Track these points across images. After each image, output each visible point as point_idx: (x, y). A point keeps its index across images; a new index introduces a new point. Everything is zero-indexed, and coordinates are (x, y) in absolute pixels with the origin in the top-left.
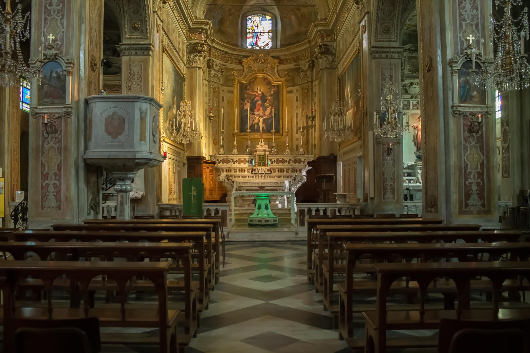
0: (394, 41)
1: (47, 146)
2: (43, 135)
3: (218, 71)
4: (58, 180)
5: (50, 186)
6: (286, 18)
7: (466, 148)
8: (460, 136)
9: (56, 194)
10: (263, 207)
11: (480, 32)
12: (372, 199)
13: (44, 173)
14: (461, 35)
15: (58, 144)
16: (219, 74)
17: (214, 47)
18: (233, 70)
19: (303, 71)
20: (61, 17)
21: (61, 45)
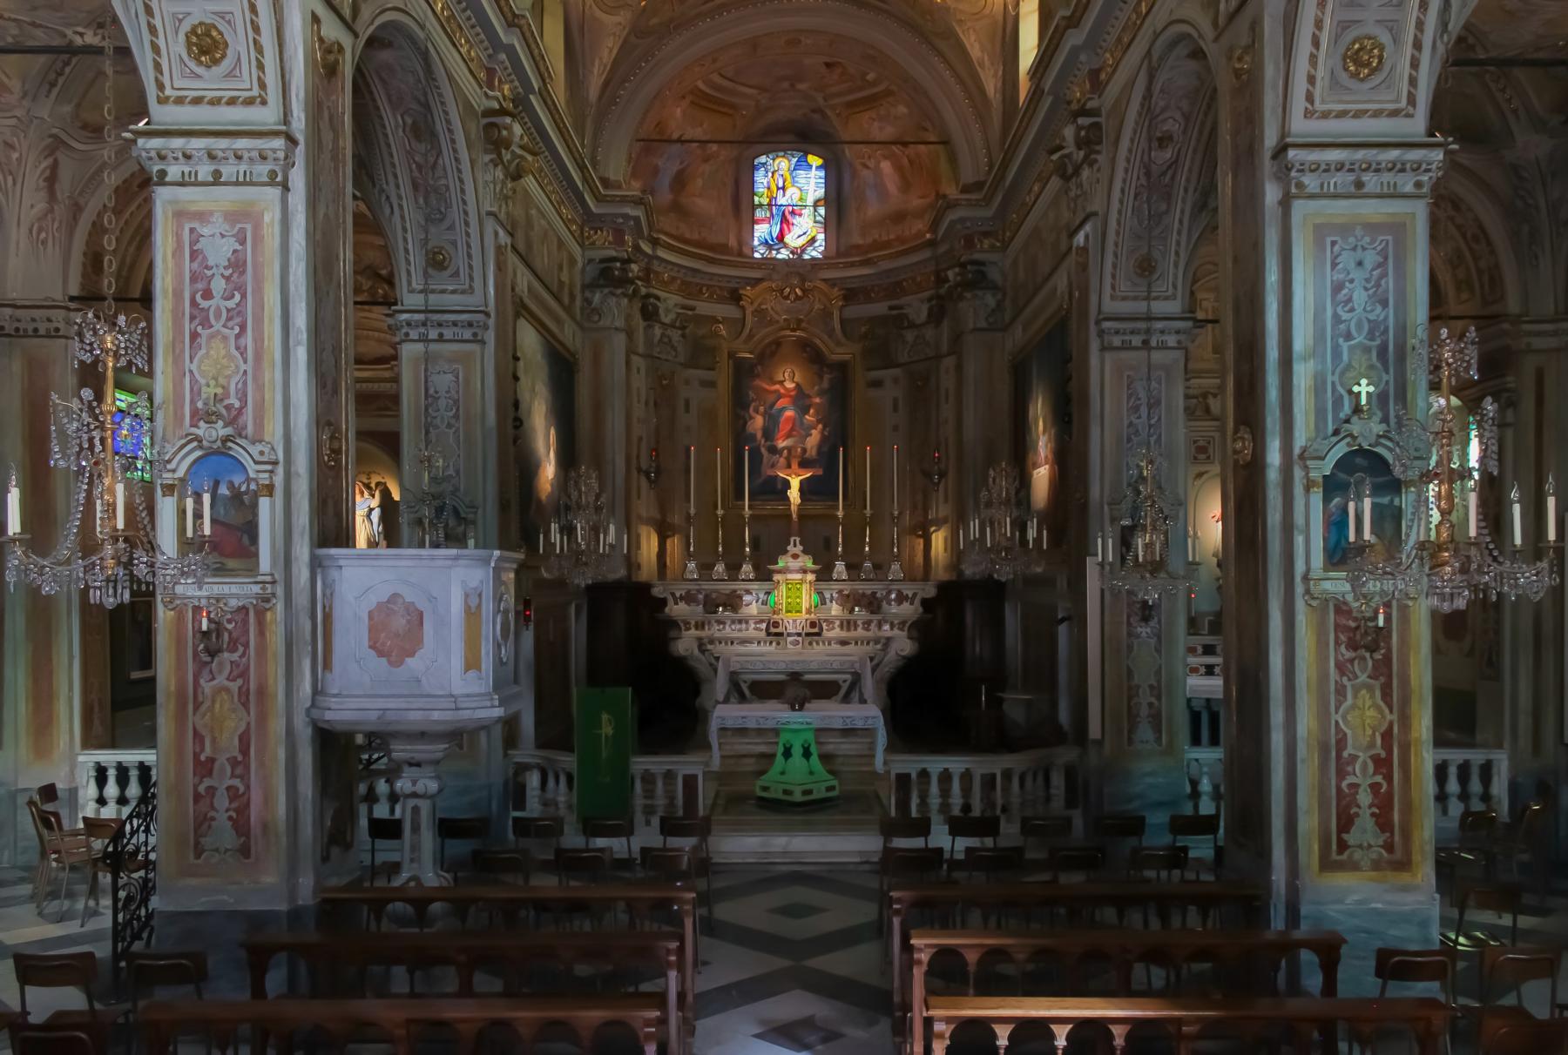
0: (1166, 298)
1: (207, 687)
2: (195, 654)
3: (672, 325)
4: (241, 777)
5: (218, 794)
6: (866, 167)
7: (1341, 691)
8: (1327, 658)
9: (234, 815)
10: (797, 751)
11: (1391, 371)
12: (1100, 743)
13: (203, 758)
14: (1336, 378)
15: (240, 682)
16: (675, 335)
17: (658, 258)
18: (714, 320)
19: (912, 326)
20: (237, 330)
21: (241, 409)
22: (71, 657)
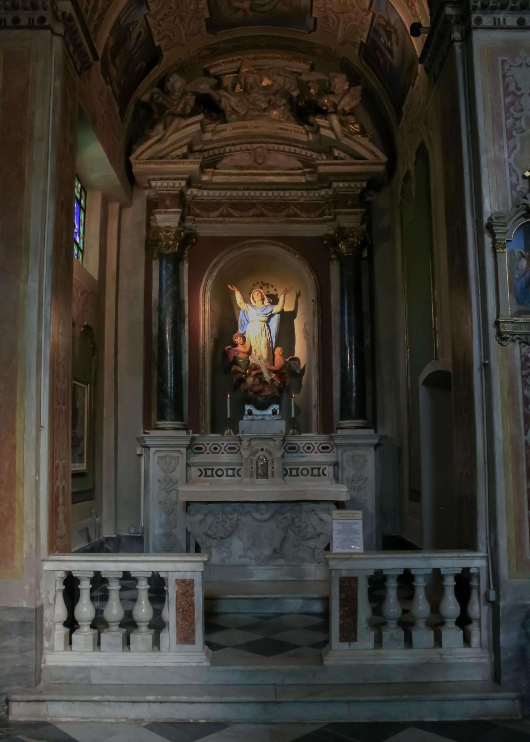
22: (39, 428)
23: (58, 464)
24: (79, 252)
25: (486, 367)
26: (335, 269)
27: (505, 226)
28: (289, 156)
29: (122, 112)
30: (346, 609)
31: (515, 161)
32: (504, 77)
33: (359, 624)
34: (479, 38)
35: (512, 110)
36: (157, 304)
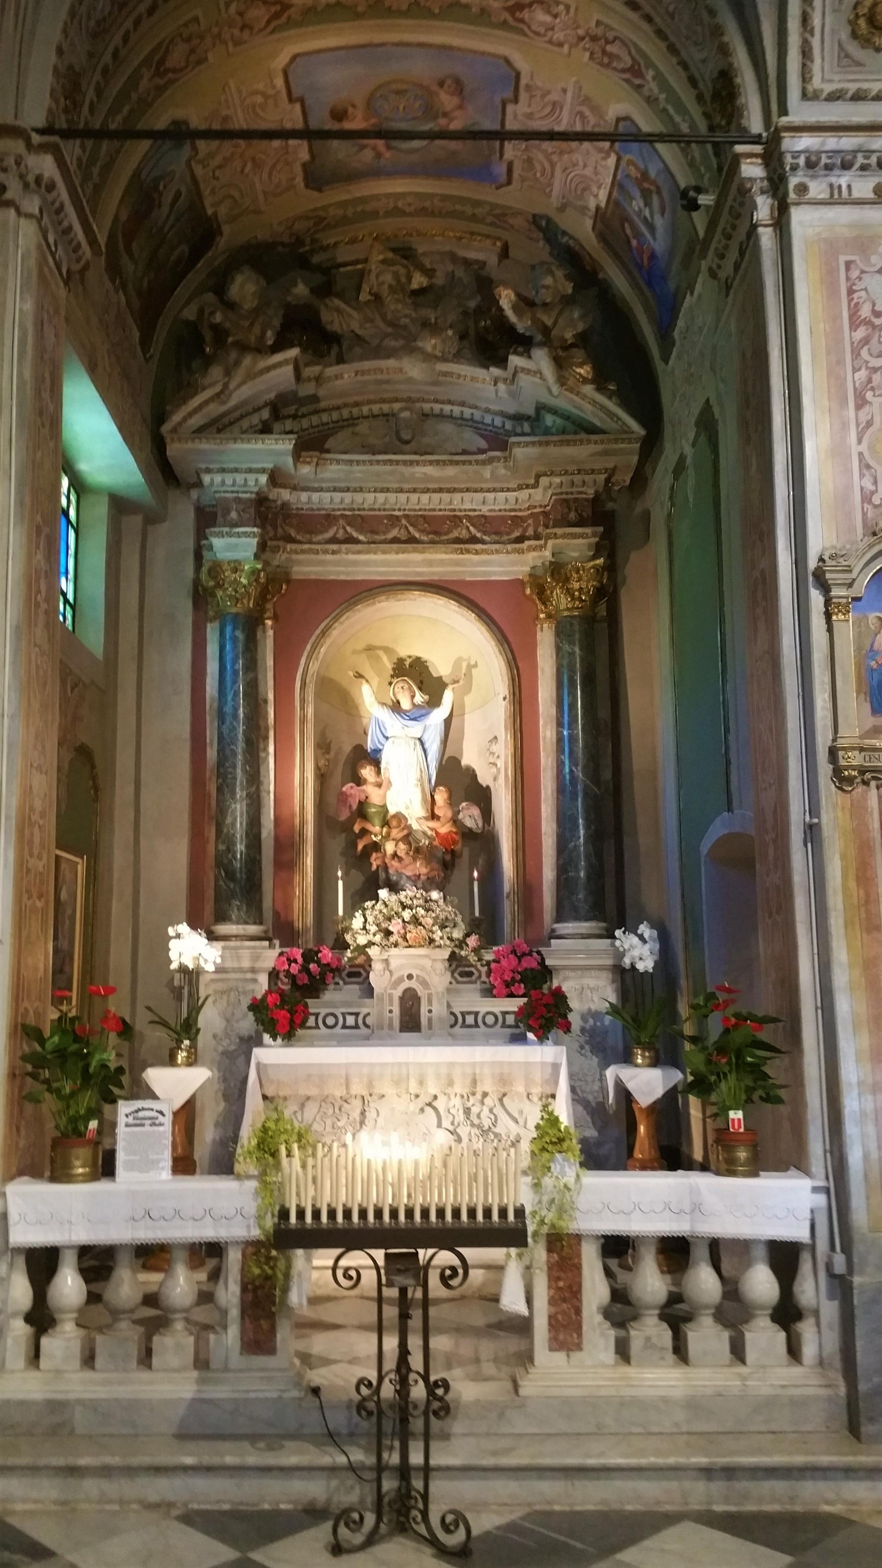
23: (26, 1009)
24: (68, 607)
25: (812, 832)
26: (545, 641)
27: (851, 571)
28: (460, 425)
29: (145, 342)
30: (561, 1284)
31: (871, 448)
32: (851, 292)
33: (585, 1313)
34: (801, 220)
35: (864, 353)
36: (216, 705)
